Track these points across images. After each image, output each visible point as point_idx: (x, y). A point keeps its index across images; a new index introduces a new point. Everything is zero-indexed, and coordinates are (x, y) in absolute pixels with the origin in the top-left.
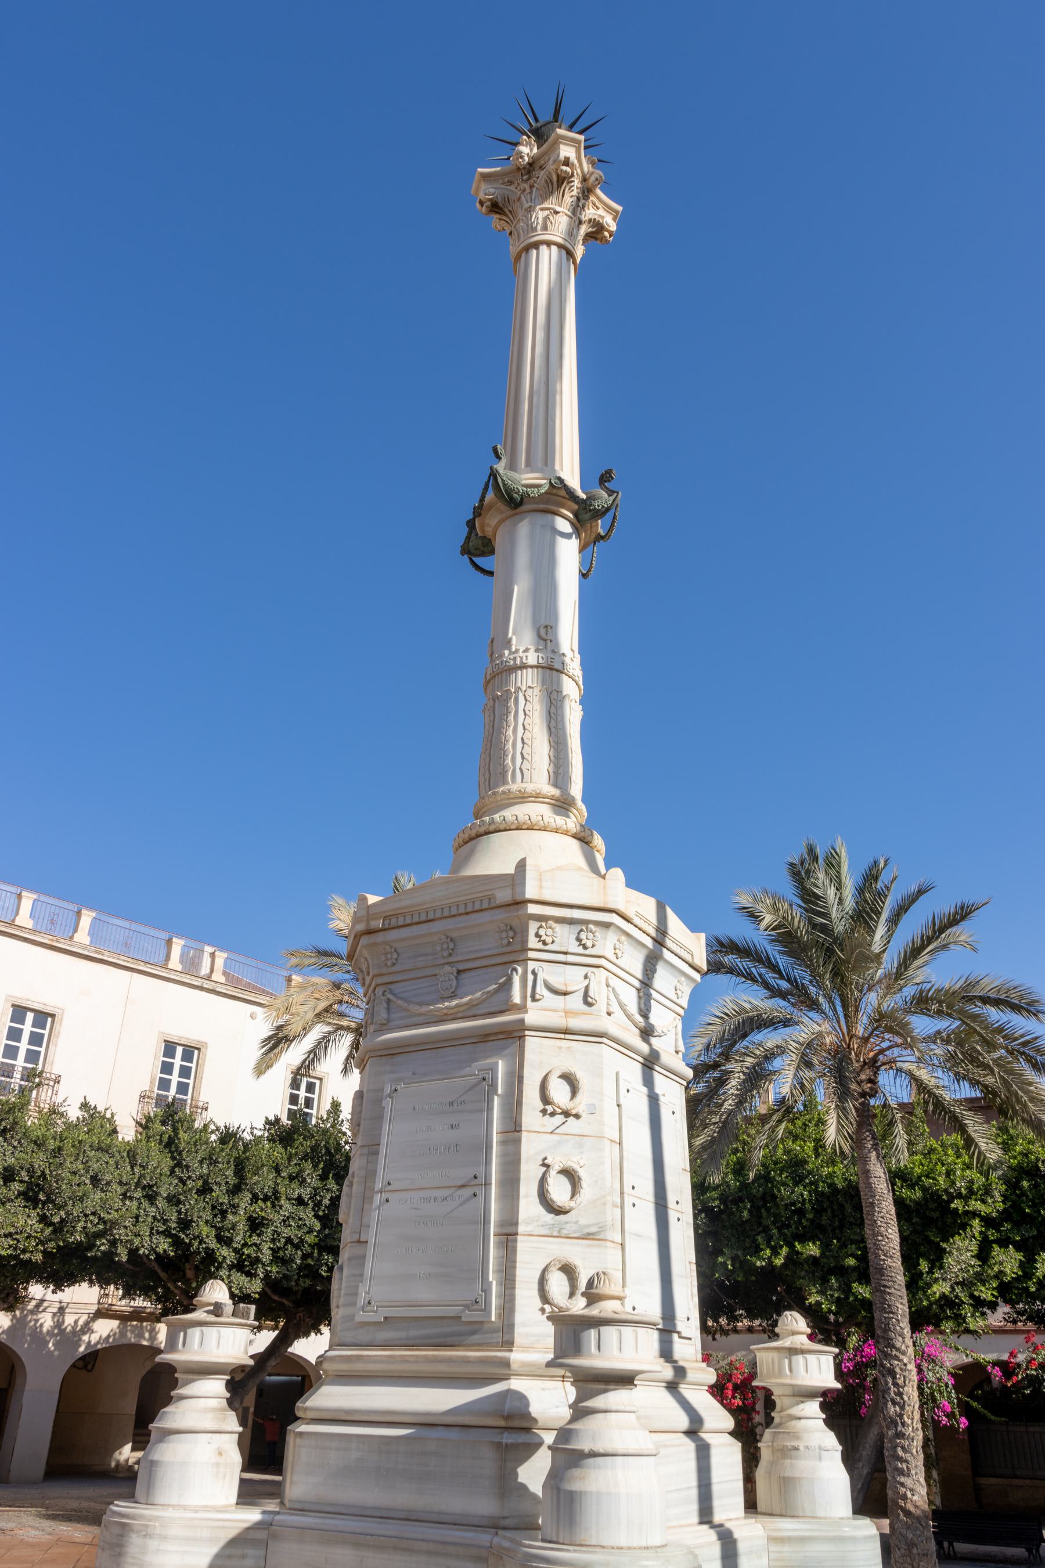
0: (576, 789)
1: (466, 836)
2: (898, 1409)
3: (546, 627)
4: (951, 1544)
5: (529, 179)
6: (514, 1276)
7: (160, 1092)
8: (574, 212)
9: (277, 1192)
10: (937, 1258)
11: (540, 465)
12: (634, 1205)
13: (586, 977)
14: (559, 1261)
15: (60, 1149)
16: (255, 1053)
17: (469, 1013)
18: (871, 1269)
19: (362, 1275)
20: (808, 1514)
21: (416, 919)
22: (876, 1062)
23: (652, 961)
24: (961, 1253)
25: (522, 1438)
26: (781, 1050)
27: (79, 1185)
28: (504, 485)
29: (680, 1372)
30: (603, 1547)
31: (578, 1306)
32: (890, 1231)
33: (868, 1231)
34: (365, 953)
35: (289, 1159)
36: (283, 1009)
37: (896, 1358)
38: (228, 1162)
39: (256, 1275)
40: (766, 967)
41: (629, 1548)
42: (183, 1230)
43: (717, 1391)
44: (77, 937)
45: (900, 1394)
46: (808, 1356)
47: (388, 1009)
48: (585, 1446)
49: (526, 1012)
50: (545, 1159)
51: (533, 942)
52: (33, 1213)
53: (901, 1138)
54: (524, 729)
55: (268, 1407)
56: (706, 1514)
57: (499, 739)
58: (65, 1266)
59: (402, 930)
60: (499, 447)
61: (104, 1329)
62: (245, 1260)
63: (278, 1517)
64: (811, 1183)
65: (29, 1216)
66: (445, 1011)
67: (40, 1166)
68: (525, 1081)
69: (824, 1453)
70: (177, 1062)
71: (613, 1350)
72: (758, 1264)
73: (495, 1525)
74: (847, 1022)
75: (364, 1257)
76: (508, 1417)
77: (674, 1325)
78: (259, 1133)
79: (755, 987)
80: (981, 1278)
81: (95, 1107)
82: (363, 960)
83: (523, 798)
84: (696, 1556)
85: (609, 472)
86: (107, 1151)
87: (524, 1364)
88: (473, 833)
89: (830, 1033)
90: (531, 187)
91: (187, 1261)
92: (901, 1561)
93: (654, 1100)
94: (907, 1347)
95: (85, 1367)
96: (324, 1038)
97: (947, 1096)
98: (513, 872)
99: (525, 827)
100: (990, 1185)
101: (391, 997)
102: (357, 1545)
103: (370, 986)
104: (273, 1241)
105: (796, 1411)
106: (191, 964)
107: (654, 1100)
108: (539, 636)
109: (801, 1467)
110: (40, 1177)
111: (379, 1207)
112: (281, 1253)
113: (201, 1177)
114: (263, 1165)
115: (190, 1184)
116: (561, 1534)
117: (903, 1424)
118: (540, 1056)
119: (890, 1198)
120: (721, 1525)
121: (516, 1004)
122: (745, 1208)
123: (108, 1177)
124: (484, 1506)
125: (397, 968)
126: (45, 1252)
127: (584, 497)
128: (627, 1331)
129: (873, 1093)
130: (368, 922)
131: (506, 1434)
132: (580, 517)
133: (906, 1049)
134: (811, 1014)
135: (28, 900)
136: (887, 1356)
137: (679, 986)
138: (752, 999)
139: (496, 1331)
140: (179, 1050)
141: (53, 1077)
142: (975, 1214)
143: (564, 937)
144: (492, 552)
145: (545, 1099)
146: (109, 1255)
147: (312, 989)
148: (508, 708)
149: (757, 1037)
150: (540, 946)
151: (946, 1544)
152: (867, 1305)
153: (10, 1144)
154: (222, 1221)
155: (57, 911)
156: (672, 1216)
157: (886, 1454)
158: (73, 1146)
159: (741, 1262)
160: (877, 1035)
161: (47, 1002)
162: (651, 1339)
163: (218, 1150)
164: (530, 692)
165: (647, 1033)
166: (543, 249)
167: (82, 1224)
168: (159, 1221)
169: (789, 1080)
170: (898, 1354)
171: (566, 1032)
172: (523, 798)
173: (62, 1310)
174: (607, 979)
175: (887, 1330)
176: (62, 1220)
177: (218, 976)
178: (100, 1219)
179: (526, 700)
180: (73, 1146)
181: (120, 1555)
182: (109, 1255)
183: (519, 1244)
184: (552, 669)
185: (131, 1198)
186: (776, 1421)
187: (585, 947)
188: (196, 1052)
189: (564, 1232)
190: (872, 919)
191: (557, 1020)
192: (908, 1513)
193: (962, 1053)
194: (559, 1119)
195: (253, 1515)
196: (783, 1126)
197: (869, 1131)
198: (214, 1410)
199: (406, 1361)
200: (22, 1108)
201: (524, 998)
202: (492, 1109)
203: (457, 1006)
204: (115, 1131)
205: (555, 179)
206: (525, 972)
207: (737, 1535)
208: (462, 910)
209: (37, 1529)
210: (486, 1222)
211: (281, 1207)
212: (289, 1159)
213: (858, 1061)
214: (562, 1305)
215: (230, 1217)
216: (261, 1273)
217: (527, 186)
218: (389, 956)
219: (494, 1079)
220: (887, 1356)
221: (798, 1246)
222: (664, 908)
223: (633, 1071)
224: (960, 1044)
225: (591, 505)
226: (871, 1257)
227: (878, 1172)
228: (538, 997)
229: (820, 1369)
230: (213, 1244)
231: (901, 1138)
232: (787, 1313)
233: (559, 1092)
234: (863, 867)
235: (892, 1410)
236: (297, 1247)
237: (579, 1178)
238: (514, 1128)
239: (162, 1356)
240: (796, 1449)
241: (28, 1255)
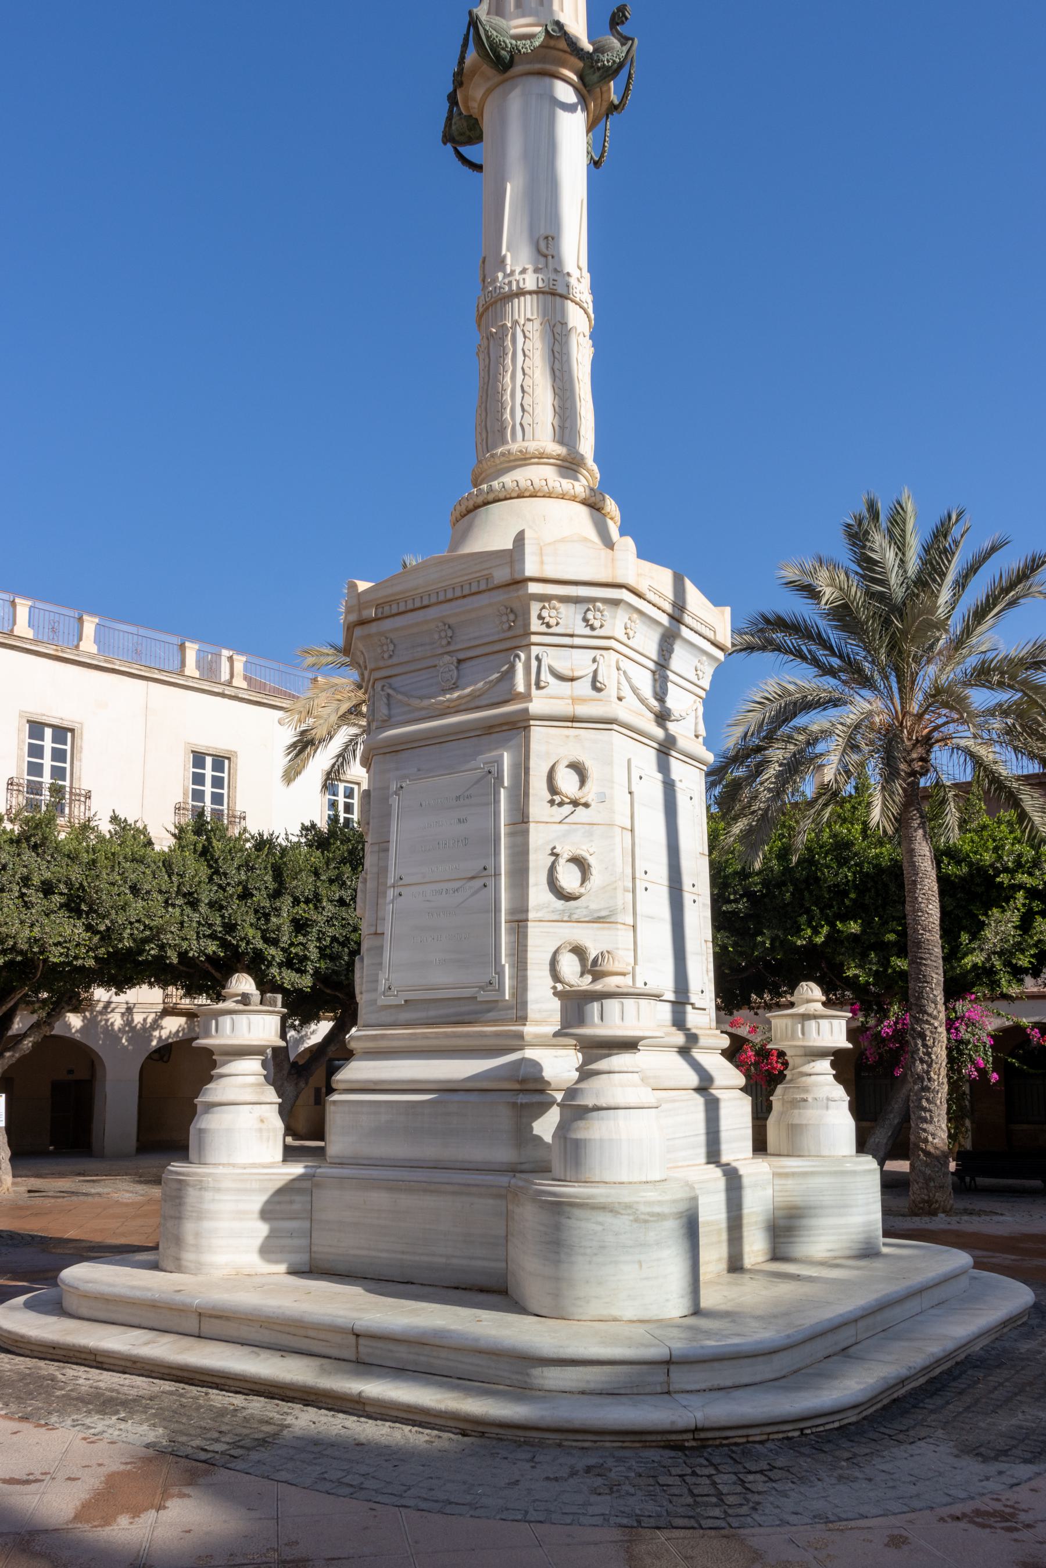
0: (587, 446)
1: (463, 508)
2: (925, 1066)
3: (547, 238)
4: (973, 1179)
6: (526, 958)
7: (195, 803)
9: (317, 894)
10: (976, 929)
11: (533, 5)
12: (646, 889)
13: (594, 660)
14: (570, 944)
15: (94, 861)
16: (282, 761)
17: (473, 705)
18: (909, 943)
19: (381, 964)
20: (812, 1154)
21: (410, 606)
22: (930, 739)
23: (668, 641)
24: (1001, 926)
25: (536, 1098)
26: (826, 734)
27: (119, 895)
28: (488, 37)
29: (692, 1039)
30: (606, 1183)
31: (585, 983)
32: (930, 906)
33: (908, 908)
34: (360, 646)
35: (327, 864)
36: (304, 714)
37: (928, 1022)
38: (266, 868)
39: (305, 972)
40: (816, 644)
41: (630, 1183)
42: (228, 933)
43: (732, 1054)
44: (83, 646)
45: (929, 1054)
47: (389, 705)
48: (589, 1101)
49: (531, 701)
50: (554, 848)
51: (535, 625)
52: (79, 923)
53: (952, 815)
54: (524, 374)
55: (304, 1084)
56: (713, 1155)
57: (497, 387)
58: (124, 969)
59: (398, 619)
61: (172, 1025)
62: (293, 958)
63: (319, 1170)
64: (856, 865)
65: (75, 926)
66: (446, 704)
67: (77, 879)
68: (531, 773)
69: (831, 1103)
70: (208, 772)
71: (614, 1020)
72: (799, 943)
73: (513, 1170)
74: (901, 698)
75: (381, 947)
76: (523, 1081)
77: (688, 998)
78: (295, 839)
79: (805, 665)
80: (1019, 947)
81: (125, 820)
82: (359, 654)
83: (525, 459)
84: (692, 1188)
85: (622, 9)
86: (142, 862)
87: (536, 1036)
88: (471, 504)
89: (882, 712)
91: (239, 961)
92: (918, 1192)
93: (669, 788)
94: (939, 1012)
95: (161, 1059)
96: (351, 741)
97: (1004, 771)
98: (511, 547)
99: (527, 494)
100: (1039, 858)
101: (390, 691)
102: (390, 1189)
103: (369, 681)
104: (319, 940)
105: (807, 1069)
106: (209, 669)
107: (669, 788)
108: (539, 251)
109: (809, 1115)
110: (78, 889)
111: (393, 901)
112: (328, 951)
113: (240, 883)
114: (301, 870)
115: (230, 890)
116: (568, 1173)
117: (930, 1080)
118: (547, 746)
119: (933, 874)
120: (728, 1164)
121: (521, 693)
123: (147, 887)
124: (503, 1154)
125: (395, 660)
126: (96, 958)
127: (589, 48)
128: (629, 1003)
129: (924, 772)
130: (360, 611)
131: (521, 1096)
132: (587, 79)
133: (962, 724)
134: (863, 692)
135: (23, 609)
136: (918, 1021)
137: (699, 666)
138: (798, 678)
139: (511, 1008)
140: (209, 761)
141: (83, 792)
142: (1021, 887)
143: (569, 618)
144: (479, 138)
145: (553, 789)
146: (160, 959)
147: (333, 690)
148: (504, 348)
149: (800, 721)
150: (543, 629)
151: (968, 1179)
152: (903, 975)
153: (43, 859)
154: (266, 924)
155: (57, 619)
156: (688, 899)
157: (912, 1105)
158: (106, 858)
159: (781, 942)
160: (932, 711)
161: (63, 716)
162: (665, 1012)
163: (253, 857)
164: (529, 325)
165: (662, 717)
167: (128, 931)
168: (203, 926)
170: (929, 1019)
171: (574, 719)
172: (525, 459)
173: (129, 1010)
174: (617, 662)
175: (920, 997)
176: (108, 929)
177: (239, 682)
178: (145, 926)
179: (525, 337)
180: (106, 858)
181: (180, 1204)
182: (160, 959)
183: (530, 930)
184: (554, 295)
185: (173, 905)
186: (788, 1077)
187: (593, 628)
188: (226, 762)
189: (575, 917)
190: (934, 581)
191: (563, 708)
192: (927, 1154)
193: (1021, 725)
194: (568, 809)
195: (297, 1169)
196: (829, 809)
197: (917, 809)
198: (252, 1085)
199: (427, 1038)
200: (49, 823)
201: (528, 685)
202: (499, 801)
203: (459, 698)
204: (150, 843)
206: (528, 658)
207: (741, 1172)
208: (458, 593)
209: (132, 1192)
210: (497, 910)
211: (323, 908)
212: (327, 864)
213: (910, 739)
214: (573, 983)
215: (274, 919)
216: (310, 968)
218: (385, 648)
219: (500, 772)
220: (918, 1021)
222: (683, 581)
223: (646, 758)
224: (1020, 715)
225: (598, 61)
226: (910, 932)
227: (924, 851)
228: (542, 684)
229: (833, 1032)
230: (260, 944)
231: (952, 815)
232: (804, 984)
233: (567, 781)
234: (932, 523)
235: (920, 1067)
236: (343, 944)
237: (589, 866)
238: (521, 819)
239: (198, 1041)
240: (805, 1100)
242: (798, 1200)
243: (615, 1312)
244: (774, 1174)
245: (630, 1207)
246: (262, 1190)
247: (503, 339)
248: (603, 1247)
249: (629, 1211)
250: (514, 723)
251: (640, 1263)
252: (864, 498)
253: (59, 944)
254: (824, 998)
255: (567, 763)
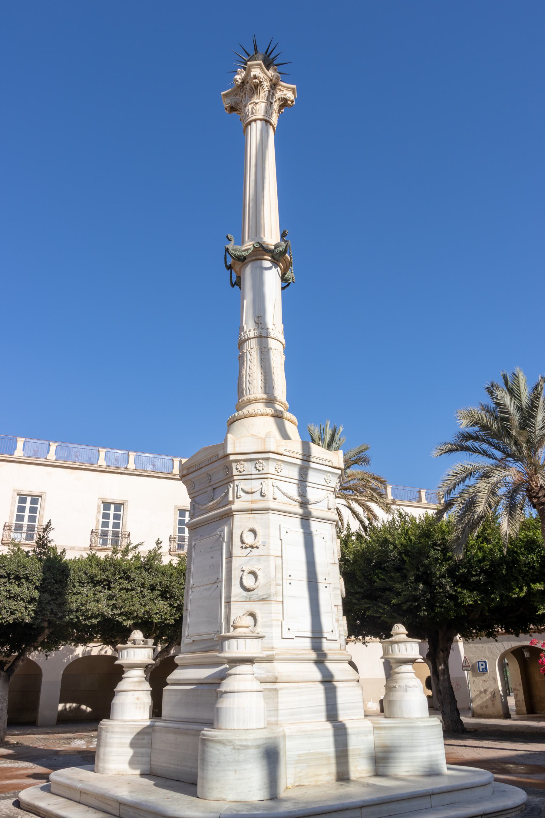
5: (243, 90)
8: (267, 100)
12: (290, 584)
13: (261, 484)
17: (217, 507)
20: (399, 716)
23: (304, 471)
30: (227, 729)
41: (238, 730)
46: (400, 644)
51: (235, 472)
52: (166, 603)
60: (229, 235)
64: (539, 552)
69: (408, 689)
72: (513, 596)
77: (322, 635)
85: (284, 231)
88: (232, 420)
90: (245, 94)
108: (255, 322)
118: (241, 523)
122: (504, 568)
126: (175, 620)
128: (241, 641)
137: (326, 478)
143: (249, 468)
145: (242, 542)
166: (253, 124)
169: (483, 503)
172: (250, 402)
184: (263, 337)
189: (252, 599)
191: (247, 506)
203: (213, 504)
205: (253, 87)
217: (243, 94)
219: (224, 535)
221: (532, 586)
228: (238, 496)
233: (249, 539)
238: (230, 556)
240: (395, 687)
241: (168, 621)
242: (388, 743)
243: (224, 796)
244: (375, 728)
245: (231, 742)
246: (131, 733)
247: (243, 357)
248: (219, 762)
249: (230, 744)
250: (229, 514)
251: (235, 771)
252: (501, 373)
253: (156, 614)
254: (407, 632)
255: (248, 529)
